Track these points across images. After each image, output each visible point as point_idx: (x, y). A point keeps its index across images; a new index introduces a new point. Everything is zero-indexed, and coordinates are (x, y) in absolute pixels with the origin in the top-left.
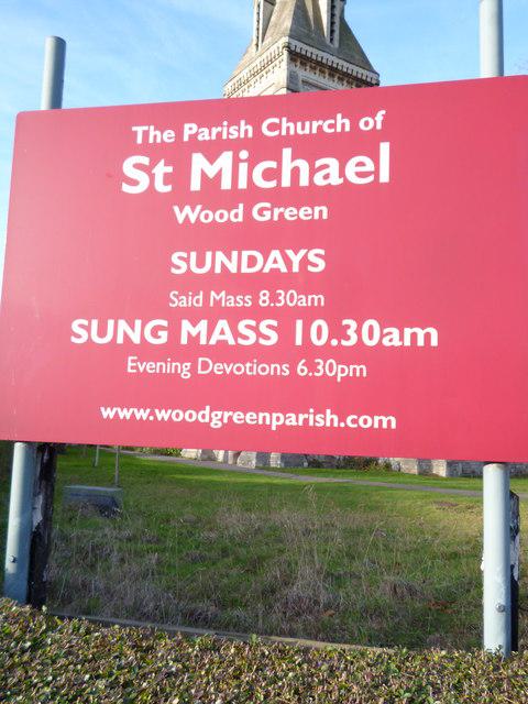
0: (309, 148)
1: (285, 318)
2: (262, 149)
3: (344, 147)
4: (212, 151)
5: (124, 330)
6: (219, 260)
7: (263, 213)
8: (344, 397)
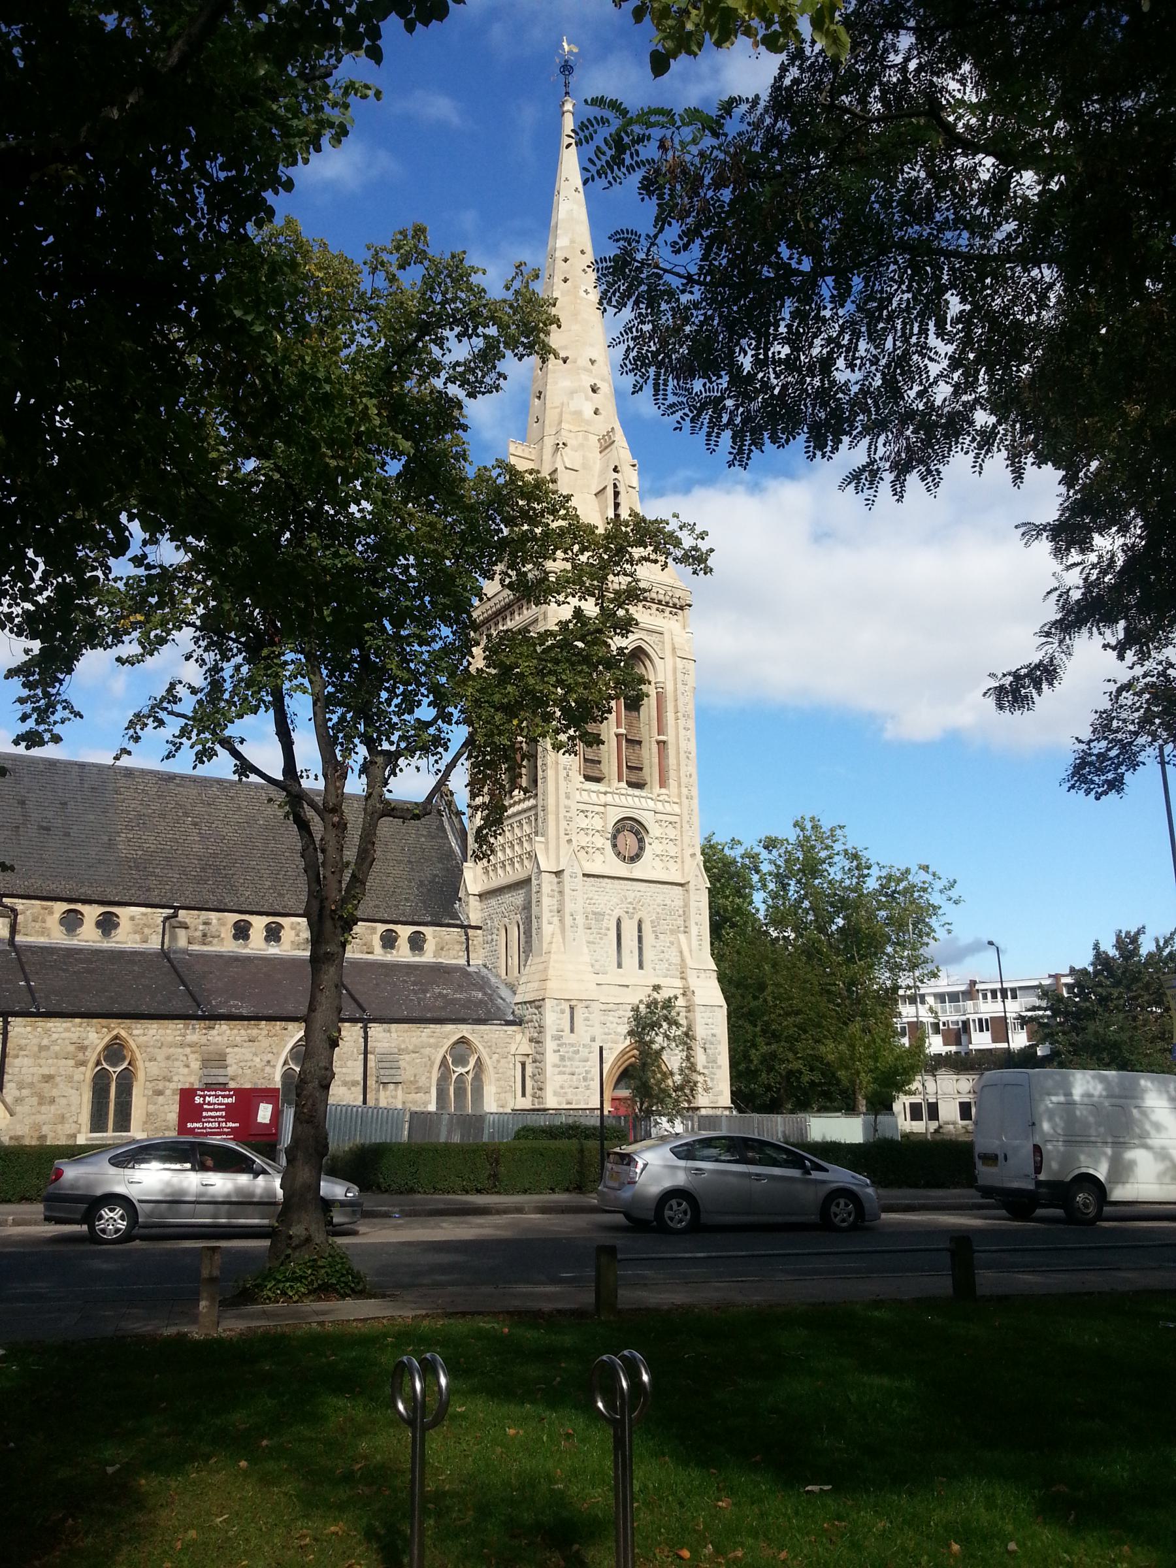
0: (223, 1096)
2: (217, 1096)
3: (228, 1096)
5: (195, 1125)
6: (210, 1114)
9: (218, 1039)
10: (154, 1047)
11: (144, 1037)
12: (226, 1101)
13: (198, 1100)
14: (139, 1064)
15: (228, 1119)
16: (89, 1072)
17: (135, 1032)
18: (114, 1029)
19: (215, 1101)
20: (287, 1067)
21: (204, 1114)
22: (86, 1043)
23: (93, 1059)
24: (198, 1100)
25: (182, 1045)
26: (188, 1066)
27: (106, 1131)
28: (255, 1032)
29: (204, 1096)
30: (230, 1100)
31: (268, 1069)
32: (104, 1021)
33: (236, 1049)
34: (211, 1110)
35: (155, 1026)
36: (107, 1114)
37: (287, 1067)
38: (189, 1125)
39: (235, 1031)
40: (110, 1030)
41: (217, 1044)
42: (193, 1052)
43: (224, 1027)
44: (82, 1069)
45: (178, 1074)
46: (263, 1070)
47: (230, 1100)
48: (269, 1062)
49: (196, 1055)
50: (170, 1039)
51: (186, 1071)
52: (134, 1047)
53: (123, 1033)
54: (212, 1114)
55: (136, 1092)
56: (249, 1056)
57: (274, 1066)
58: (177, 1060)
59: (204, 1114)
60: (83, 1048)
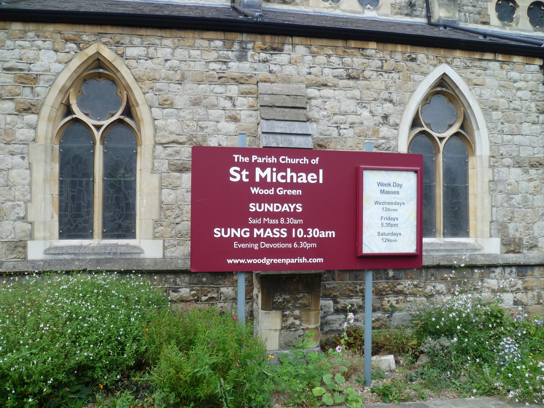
0: (297, 169)
1: (289, 228)
2: (281, 168)
3: (308, 169)
4: (263, 167)
5: (233, 232)
6: (266, 207)
7: (281, 192)
8: (308, 253)
9: (290, 70)
10: (169, 80)
11: (138, 59)
12: (303, 178)
13: (236, 175)
14: (142, 111)
15: (309, 220)
16: (46, 127)
17: (131, 52)
18: (88, 44)
19: (278, 177)
20: (418, 130)
21: (253, 207)
22: (36, 68)
23: (51, 100)
24: (236, 175)
25: (222, 80)
26: (235, 119)
27: (90, 236)
28: (356, 61)
29: (251, 167)
30: (311, 178)
31: (385, 131)
32: (69, 31)
33: (326, 92)
34: (269, 199)
35: (168, 42)
36: (90, 204)
37: (418, 130)
38: (218, 233)
39: (322, 59)
40: (81, 46)
41: (287, 80)
42: (244, 94)
43: (301, 50)
44: (30, 118)
45: (217, 131)
46: (376, 132)
47: (311, 178)
48: (386, 117)
49: (250, 100)
50: (199, 66)
51: (231, 127)
52: (129, 79)
53: (107, 53)
54: (272, 208)
55: (143, 163)
56: (350, 105)
57: (396, 126)
58: (214, 106)
59: (253, 207)
60: (29, 80)
